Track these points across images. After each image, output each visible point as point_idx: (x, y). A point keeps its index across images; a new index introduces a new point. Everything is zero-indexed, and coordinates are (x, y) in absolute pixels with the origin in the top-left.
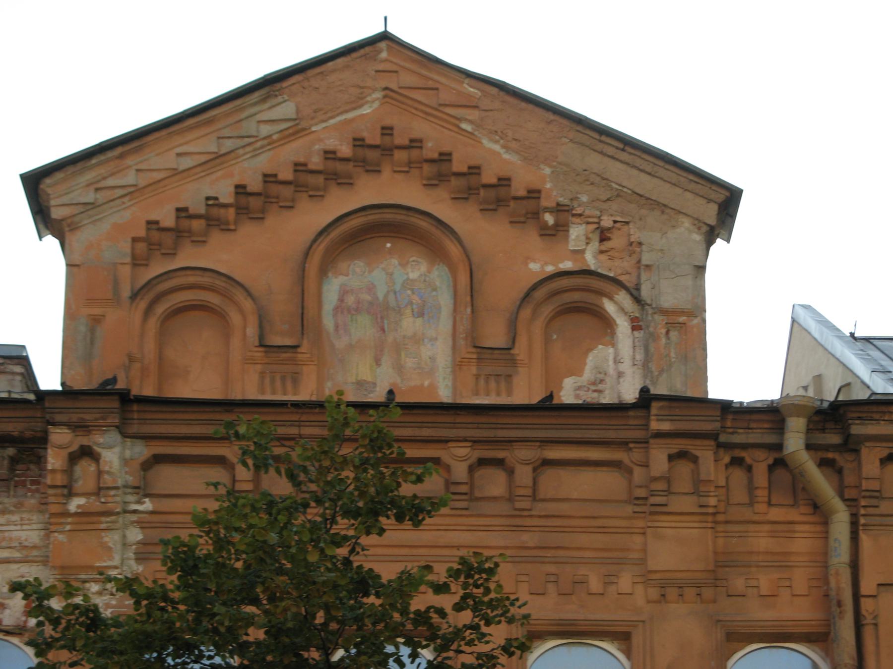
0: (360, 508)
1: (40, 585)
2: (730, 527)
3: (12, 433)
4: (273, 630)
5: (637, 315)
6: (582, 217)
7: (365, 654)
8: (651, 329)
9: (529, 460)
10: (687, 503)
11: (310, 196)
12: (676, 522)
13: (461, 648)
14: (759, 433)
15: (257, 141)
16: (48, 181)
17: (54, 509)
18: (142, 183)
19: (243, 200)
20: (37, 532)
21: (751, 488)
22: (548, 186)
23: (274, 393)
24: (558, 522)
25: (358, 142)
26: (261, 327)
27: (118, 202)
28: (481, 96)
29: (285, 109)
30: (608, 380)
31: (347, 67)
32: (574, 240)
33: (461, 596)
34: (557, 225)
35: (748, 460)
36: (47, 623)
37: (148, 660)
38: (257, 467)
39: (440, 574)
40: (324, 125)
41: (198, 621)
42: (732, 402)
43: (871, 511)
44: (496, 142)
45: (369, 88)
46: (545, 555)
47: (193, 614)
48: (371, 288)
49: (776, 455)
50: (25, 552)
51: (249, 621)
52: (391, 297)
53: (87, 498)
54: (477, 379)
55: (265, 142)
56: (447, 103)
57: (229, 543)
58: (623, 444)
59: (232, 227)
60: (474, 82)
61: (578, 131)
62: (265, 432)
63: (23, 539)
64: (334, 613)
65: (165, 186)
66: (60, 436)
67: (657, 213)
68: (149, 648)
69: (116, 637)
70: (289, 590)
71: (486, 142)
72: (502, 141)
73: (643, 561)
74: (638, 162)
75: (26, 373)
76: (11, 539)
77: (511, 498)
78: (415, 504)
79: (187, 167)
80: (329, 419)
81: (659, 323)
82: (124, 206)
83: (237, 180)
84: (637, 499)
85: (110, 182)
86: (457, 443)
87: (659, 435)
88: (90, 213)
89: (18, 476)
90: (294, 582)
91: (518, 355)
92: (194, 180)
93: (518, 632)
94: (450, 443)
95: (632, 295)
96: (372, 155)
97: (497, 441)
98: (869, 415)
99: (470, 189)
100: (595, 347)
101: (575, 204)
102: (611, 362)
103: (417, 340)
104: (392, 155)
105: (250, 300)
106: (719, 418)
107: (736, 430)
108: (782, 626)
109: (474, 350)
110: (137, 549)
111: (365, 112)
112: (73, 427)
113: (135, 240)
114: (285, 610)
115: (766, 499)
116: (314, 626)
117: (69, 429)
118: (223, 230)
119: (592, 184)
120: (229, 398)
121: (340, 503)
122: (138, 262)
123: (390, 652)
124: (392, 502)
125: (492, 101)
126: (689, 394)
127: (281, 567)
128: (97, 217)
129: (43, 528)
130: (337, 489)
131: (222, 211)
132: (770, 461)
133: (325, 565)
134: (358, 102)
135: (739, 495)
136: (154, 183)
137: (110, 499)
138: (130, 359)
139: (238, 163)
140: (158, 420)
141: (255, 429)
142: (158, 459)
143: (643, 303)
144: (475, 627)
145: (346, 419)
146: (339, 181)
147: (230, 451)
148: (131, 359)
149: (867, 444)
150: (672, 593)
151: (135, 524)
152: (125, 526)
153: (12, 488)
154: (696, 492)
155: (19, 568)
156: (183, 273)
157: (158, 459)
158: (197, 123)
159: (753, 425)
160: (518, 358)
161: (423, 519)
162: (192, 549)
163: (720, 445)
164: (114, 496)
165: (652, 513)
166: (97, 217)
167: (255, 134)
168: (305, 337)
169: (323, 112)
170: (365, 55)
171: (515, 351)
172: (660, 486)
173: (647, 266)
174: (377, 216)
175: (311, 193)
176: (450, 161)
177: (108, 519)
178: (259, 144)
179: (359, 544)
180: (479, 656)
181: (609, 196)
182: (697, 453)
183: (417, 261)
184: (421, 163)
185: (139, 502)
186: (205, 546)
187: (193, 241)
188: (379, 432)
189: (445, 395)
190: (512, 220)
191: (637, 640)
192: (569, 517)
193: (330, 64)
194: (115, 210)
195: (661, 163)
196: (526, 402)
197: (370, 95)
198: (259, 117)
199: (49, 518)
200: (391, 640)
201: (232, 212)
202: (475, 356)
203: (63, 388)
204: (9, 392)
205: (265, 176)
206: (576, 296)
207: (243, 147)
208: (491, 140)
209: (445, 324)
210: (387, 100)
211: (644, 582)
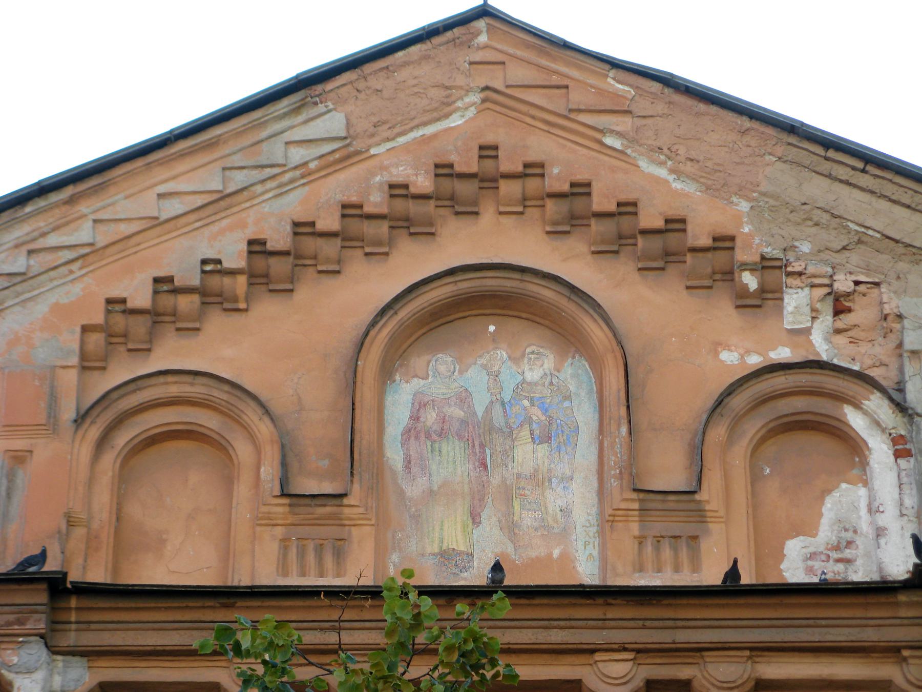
15: (285, 172)
18: (101, 241)
31: (426, 57)
44: (662, 164)
59: (242, 305)
83: (251, 232)
85: (53, 240)
88: (18, 288)
91: (708, 502)
119: (817, 224)
156: (162, 379)
160: (707, 508)
181: (845, 243)
194: (56, 283)
202: (636, 506)
206: (799, 404)
207: (263, 181)
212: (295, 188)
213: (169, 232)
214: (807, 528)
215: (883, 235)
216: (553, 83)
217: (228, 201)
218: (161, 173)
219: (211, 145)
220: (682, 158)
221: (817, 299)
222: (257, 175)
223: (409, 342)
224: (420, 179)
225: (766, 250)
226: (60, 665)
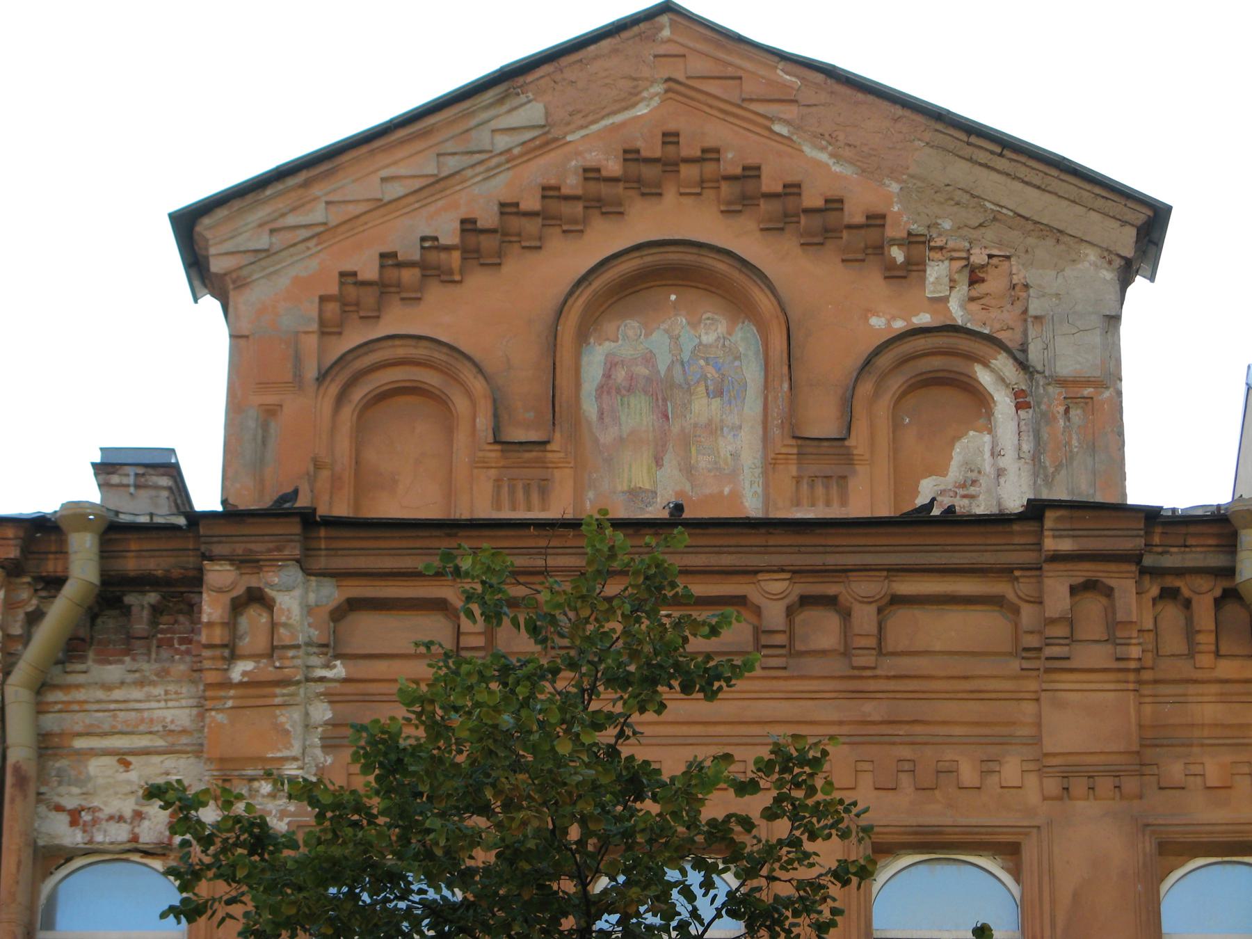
0: (629, 673)
1: (185, 789)
2: (1163, 689)
3: (155, 572)
4: (508, 852)
5: (1024, 388)
6: (944, 251)
7: (637, 883)
8: (1043, 407)
9: (873, 597)
10: (1098, 655)
11: (564, 232)
13: (775, 874)
14: (1201, 552)
16: (207, 221)
17: (211, 677)
19: (472, 240)
20: (187, 711)
21: (1190, 632)
22: (896, 209)
23: (514, 509)
25: (631, 155)
26: (496, 416)
27: (301, 247)
28: (800, 87)
29: (530, 112)
30: (983, 480)
31: (615, 51)
32: (933, 283)
33: (774, 798)
34: (908, 262)
35: (1186, 592)
36: (194, 842)
37: (335, 897)
38: (487, 618)
39: (743, 768)
40: (583, 132)
41: (405, 840)
42: (1161, 508)
44: (823, 149)
45: (647, 79)
46: (896, 733)
47: (397, 830)
48: (649, 359)
49: (1226, 584)
50: (170, 739)
51: (474, 839)
52: (677, 370)
53: (255, 662)
54: (798, 482)
57: (448, 728)
58: (1006, 572)
59: (457, 278)
60: (790, 67)
61: (936, 130)
62: (498, 568)
63: (168, 720)
64: (592, 827)
65: (366, 223)
66: (219, 575)
67: (1050, 242)
68: (337, 882)
69: (290, 865)
70: (531, 793)
71: (809, 150)
72: (830, 148)
73: (1037, 740)
74: (1022, 172)
75: (174, 488)
77: (846, 652)
78: (710, 668)
79: (395, 196)
80: (589, 550)
81: (1054, 398)
83: (463, 212)
84: (1026, 649)
85: (291, 220)
86: (771, 574)
87: (1057, 558)
88: (263, 263)
89: (162, 631)
90: (536, 782)
91: (856, 447)
93: (857, 852)
94: (760, 575)
95: (1015, 359)
96: (649, 172)
97: (826, 571)
99: (786, 215)
100: (966, 433)
101: (934, 234)
102: (987, 455)
103: (713, 429)
104: (678, 171)
105: (480, 377)
106: (1142, 533)
107: (1167, 549)
109: (793, 442)
110: (323, 731)
111: (639, 114)
112: (237, 562)
113: (323, 299)
114: (524, 823)
115: (1213, 648)
116: (565, 846)
117: (232, 565)
118: (443, 282)
119: (957, 204)
120: (452, 517)
121: (602, 667)
122: (327, 330)
123: (673, 880)
124: (677, 665)
125: (816, 93)
126: (1099, 498)
127: (519, 761)
128: (272, 269)
129: (195, 704)
130: (599, 647)
131: (444, 256)
132: (1218, 592)
133: (580, 758)
134: (631, 98)
135: (1174, 642)
136: (350, 220)
137: (287, 663)
138: (315, 465)
139: (465, 188)
141: (484, 564)
142: (354, 605)
143: (1031, 369)
144: (795, 843)
145: (612, 548)
146: (604, 210)
147: (450, 592)
148: (318, 465)
150: (1079, 785)
151: (322, 697)
152: (308, 701)
153: (154, 649)
154: (1111, 640)
155: (162, 762)
156: (390, 343)
157: (354, 605)
159: (1190, 541)
161: (720, 689)
162: (394, 737)
163: (1144, 571)
164: (293, 658)
165: (1047, 671)
167: (488, 147)
168: (557, 428)
169: (581, 115)
170: (640, 34)
172: (1060, 631)
173: (1036, 318)
174: (657, 258)
175: (565, 227)
176: (759, 177)
177: (285, 691)
178: (494, 162)
179: (630, 726)
180: (801, 885)
182: (1112, 582)
183: (712, 319)
184: (718, 181)
185: (328, 666)
186: (413, 735)
187: (403, 299)
188: (657, 566)
189: (752, 506)
190: (845, 257)
191: (1029, 854)
193: (592, 48)
194: (295, 258)
195: (1055, 172)
196: (866, 514)
197: (646, 89)
198: (494, 124)
199: (204, 691)
200: (675, 862)
201: (456, 255)
203: (224, 507)
204: (151, 515)
205: (502, 205)
206: (937, 362)
207: (473, 166)
208: (815, 146)
209: (752, 406)
210: (670, 95)
211: (1039, 770)
215: (1015, 213)
217: (442, 184)
218: (383, 159)
221: (955, 271)
225: (912, 227)
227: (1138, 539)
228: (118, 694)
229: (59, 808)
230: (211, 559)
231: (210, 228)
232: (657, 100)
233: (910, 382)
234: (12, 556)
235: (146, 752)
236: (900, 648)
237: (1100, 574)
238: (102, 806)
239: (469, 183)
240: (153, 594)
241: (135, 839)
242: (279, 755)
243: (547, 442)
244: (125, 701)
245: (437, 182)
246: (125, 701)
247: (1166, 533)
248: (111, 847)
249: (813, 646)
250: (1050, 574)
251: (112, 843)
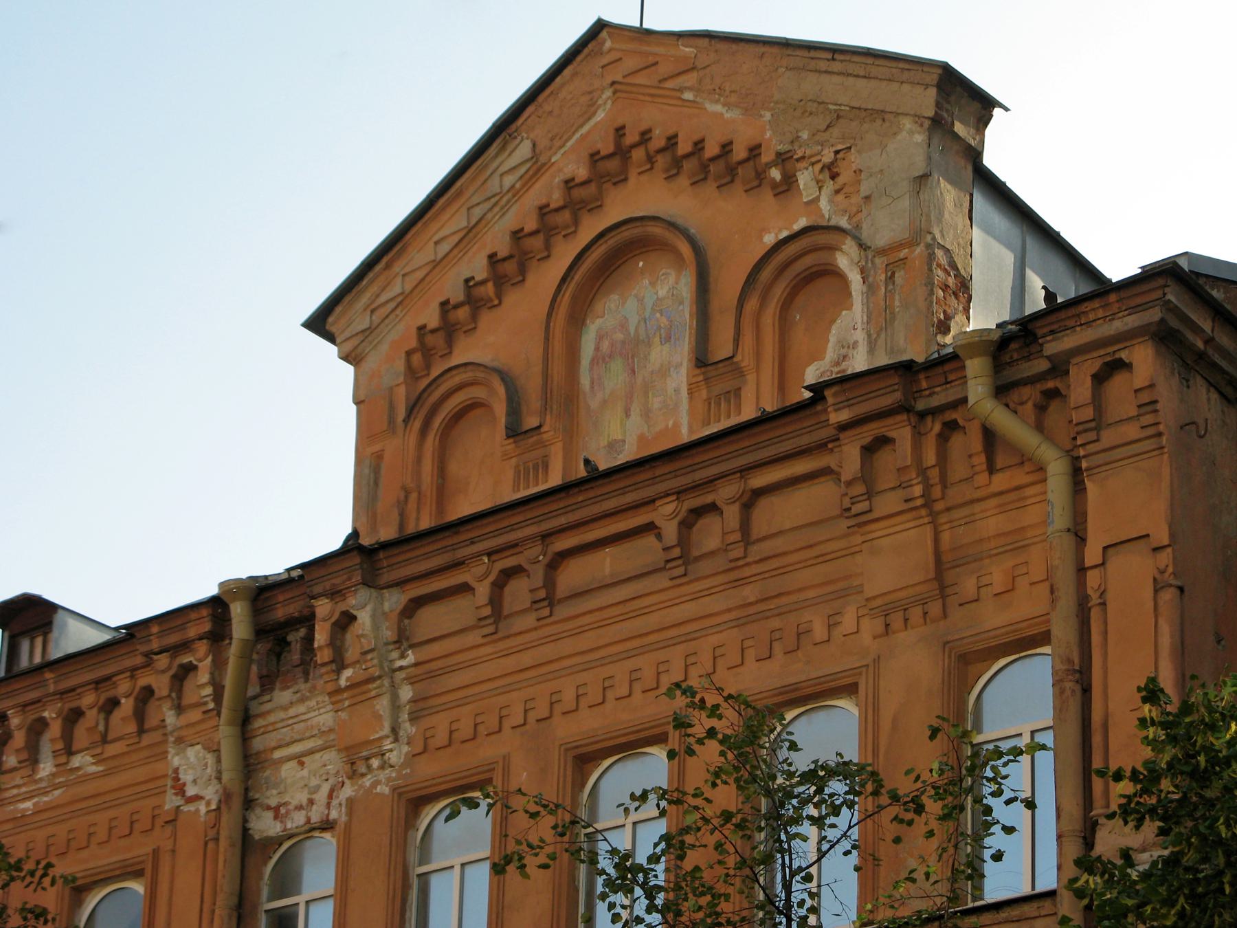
2: (956, 514)
8: (871, 279)
12: (886, 528)
15: (502, 197)
18: (408, 288)
22: (768, 134)
24: (774, 563)
31: (575, 74)
40: (562, 151)
43: (1091, 448)
44: (717, 101)
46: (769, 608)
55: (510, 195)
56: (666, 76)
59: (496, 302)
61: (789, 55)
66: (323, 607)
74: (851, 68)
76: (312, 727)
82: (399, 318)
83: (488, 251)
85: (383, 299)
87: (843, 427)
88: (370, 338)
91: (742, 360)
92: (452, 266)
98: (1062, 324)
107: (932, 390)
108: (1015, 631)
110: (410, 708)
111: (599, 119)
117: (327, 598)
119: (811, 114)
128: (376, 341)
137: (369, 664)
140: (613, 491)
146: (588, 208)
149: (1074, 361)
150: (897, 620)
155: (321, 757)
156: (449, 375)
157: (417, 603)
158: (447, 200)
159: (951, 378)
160: (742, 365)
164: (372, 659)
166: (376, 341)
171: (738, 358)
177: (375, 685)
181: (828, 122)
185: (403, 656)
192: (785, 554)
193: (558, 80)
194: (390, 327)
202: (701, 378)
206: (808, 261)
207: (491, 209)
210: (618, 94)
212: (511, 206)
213: (445, 268)
214: (817, 355)
215: (850, 107)
216: (650, 63)
217: (474, 231)
218: (434, 226)
219: (459, 194)
220: (727, 93)
221: (818, 173)
222: (487, 205)
223: (594, 291)
224: (581, 170)
225: (779, 148)
226: (387, 595)
227: (896, 393)
228: (292, 712)
229: (269, 808)
230: (313, 598)
231: (335, 323)
232: (610, 102)
233: (792, 285)
234: (207, 630)
235: (311, 752)
236: (763, 534)
237: (883, 430)
238: (290, 801)
239: (492, 223)
240: (302, 630)
241: (308, 821)
242: (377, 736)
243: (540, 427)
244: (297, 716)
245: (470, 231)
246: (297, 716)
247: (928, 377)
248: (298, 831)
249: (705, 550)
250: (846, 441)
251: (297, 827)
